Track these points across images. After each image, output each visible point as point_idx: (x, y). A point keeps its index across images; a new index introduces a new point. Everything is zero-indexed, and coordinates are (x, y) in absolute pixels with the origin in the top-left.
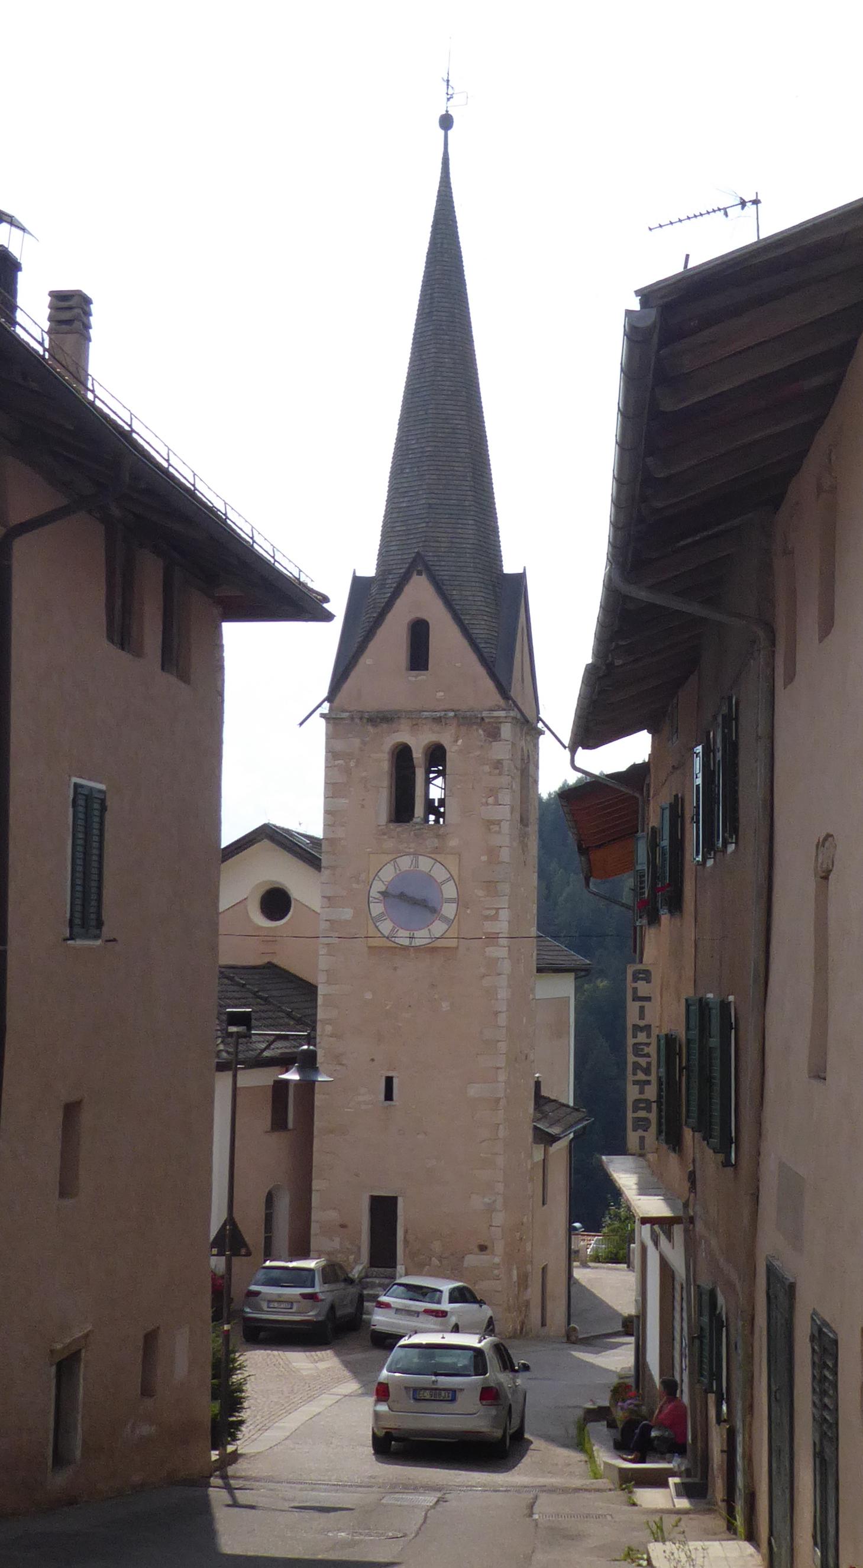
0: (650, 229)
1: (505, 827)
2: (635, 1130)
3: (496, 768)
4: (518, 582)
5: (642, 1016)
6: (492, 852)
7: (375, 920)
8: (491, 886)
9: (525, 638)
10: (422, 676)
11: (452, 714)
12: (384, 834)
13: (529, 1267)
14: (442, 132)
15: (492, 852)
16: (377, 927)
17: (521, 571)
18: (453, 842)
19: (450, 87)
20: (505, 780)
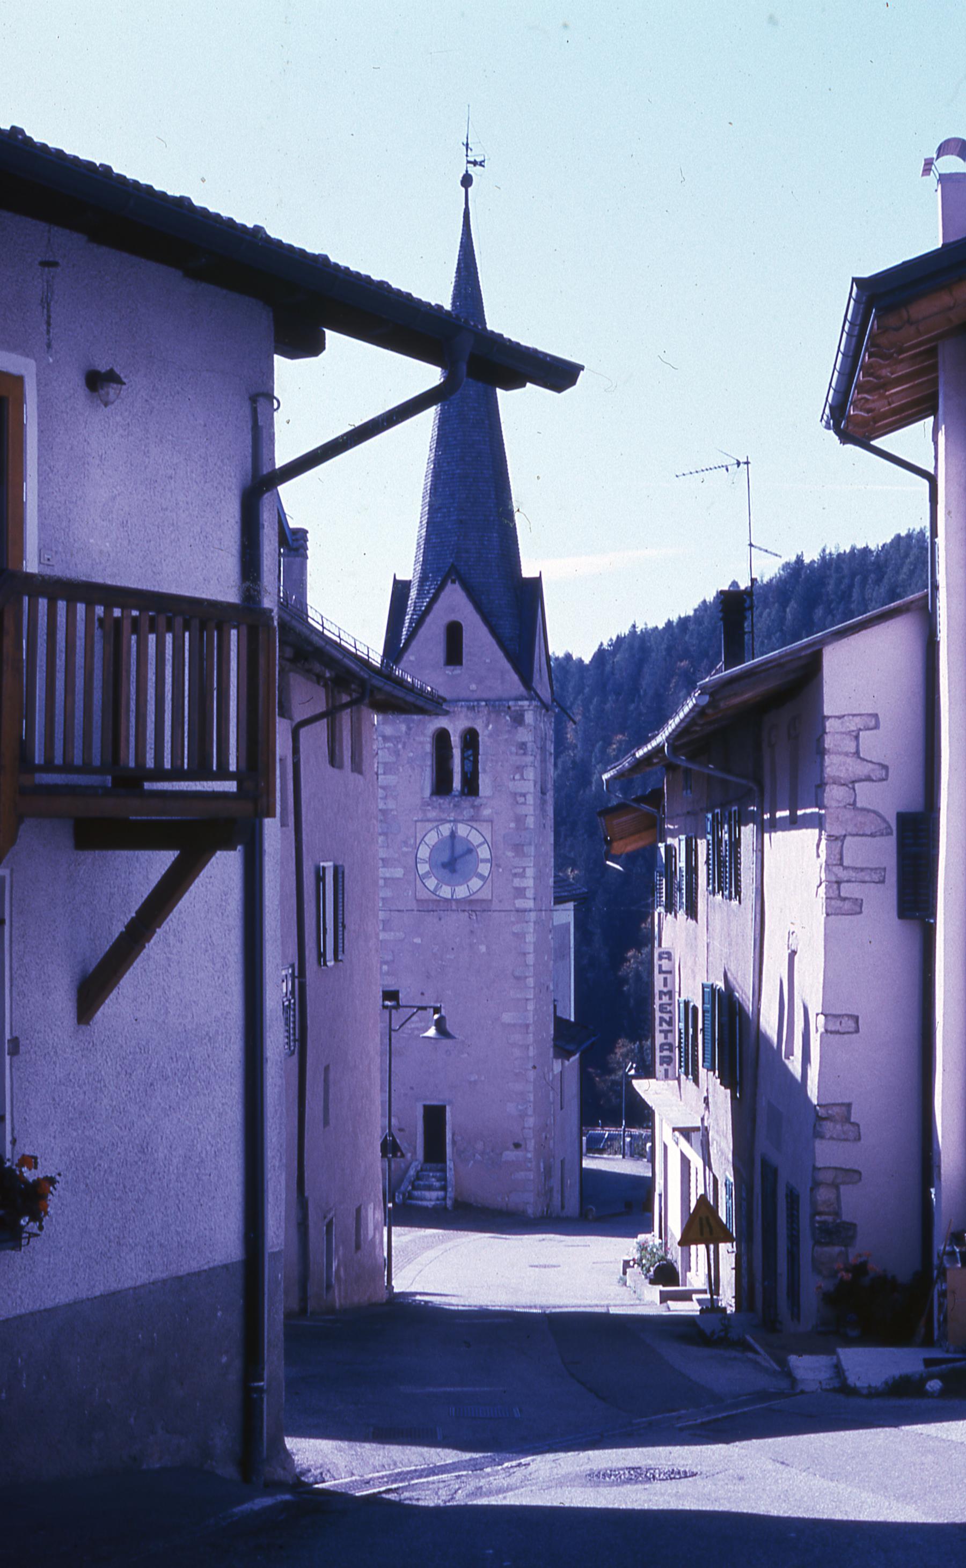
0: (677, 476)
1: (530, 799)
2: (661, 1064)
3: (521, 748)
4: (535, 585)
5: (665, 985)
6: (520, 820)
7: (422, 878)
8: (518, 848)
9: (542, 641)
10: (457, 671)
11: (483, 703)
12: (429, 805)
13: (552, 1160)
14: (463, 190)
15: (520, 820)
16: (424, 884)
17: (538, 575)
18: (486, 812)
19: (469, 150)
20: (529, 759)
